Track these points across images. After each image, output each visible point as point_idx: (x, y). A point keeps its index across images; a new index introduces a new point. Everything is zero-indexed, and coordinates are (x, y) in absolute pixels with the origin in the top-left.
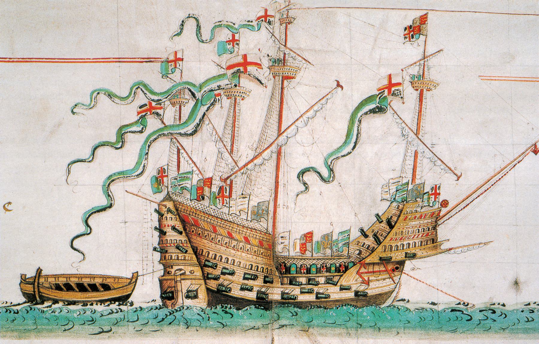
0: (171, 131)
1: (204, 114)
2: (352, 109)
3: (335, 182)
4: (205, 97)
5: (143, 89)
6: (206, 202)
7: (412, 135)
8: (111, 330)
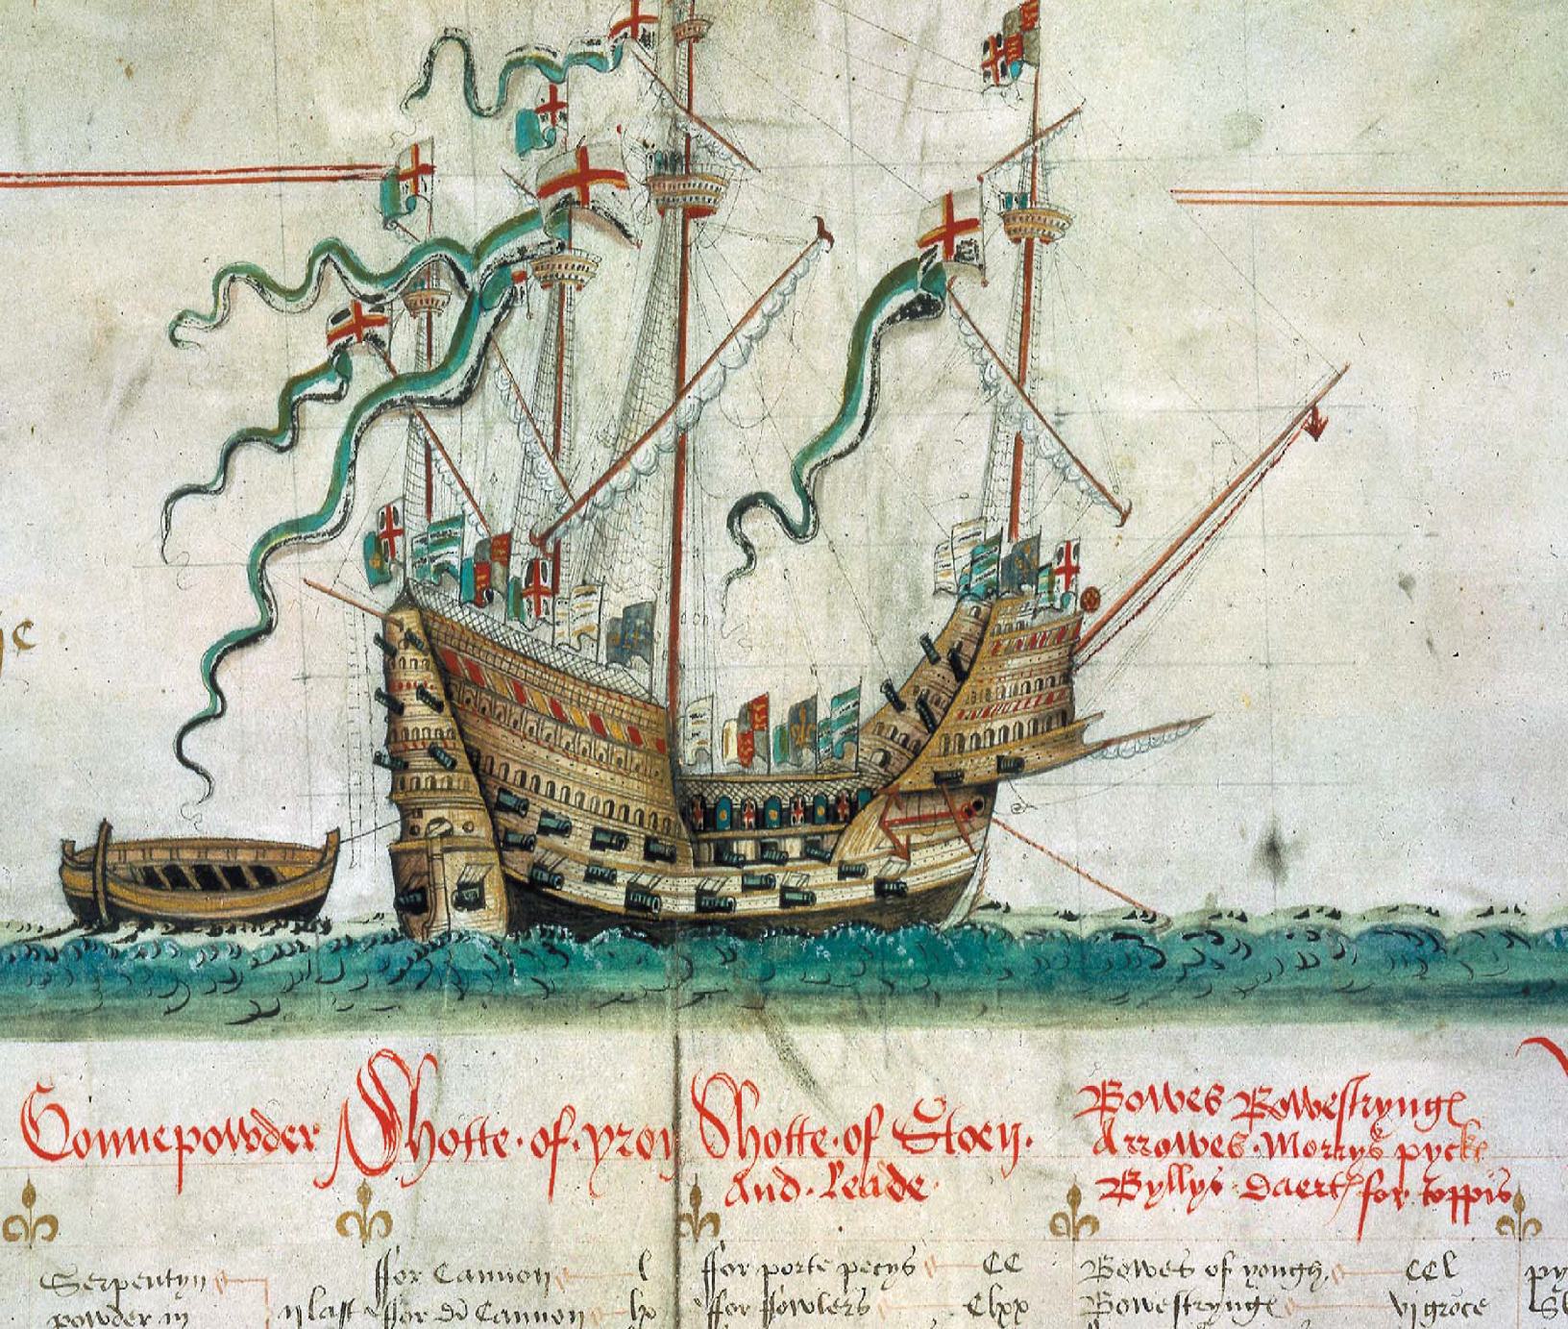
0: (409, 394)
1: (489, 338)
2: (857, 306)
3: (821, 540)
4: (486, 282)
5: (340, 264)
6: (498, 612)
7: (1006, 383)
8: (276, 1011)
